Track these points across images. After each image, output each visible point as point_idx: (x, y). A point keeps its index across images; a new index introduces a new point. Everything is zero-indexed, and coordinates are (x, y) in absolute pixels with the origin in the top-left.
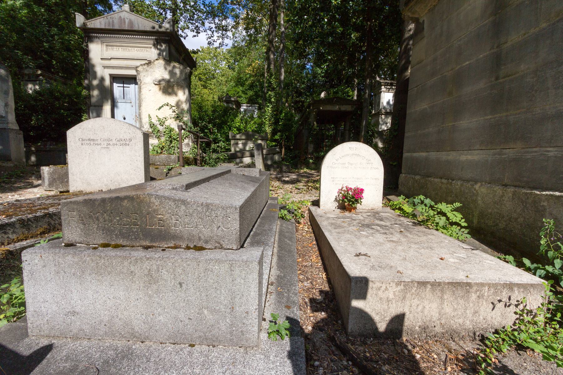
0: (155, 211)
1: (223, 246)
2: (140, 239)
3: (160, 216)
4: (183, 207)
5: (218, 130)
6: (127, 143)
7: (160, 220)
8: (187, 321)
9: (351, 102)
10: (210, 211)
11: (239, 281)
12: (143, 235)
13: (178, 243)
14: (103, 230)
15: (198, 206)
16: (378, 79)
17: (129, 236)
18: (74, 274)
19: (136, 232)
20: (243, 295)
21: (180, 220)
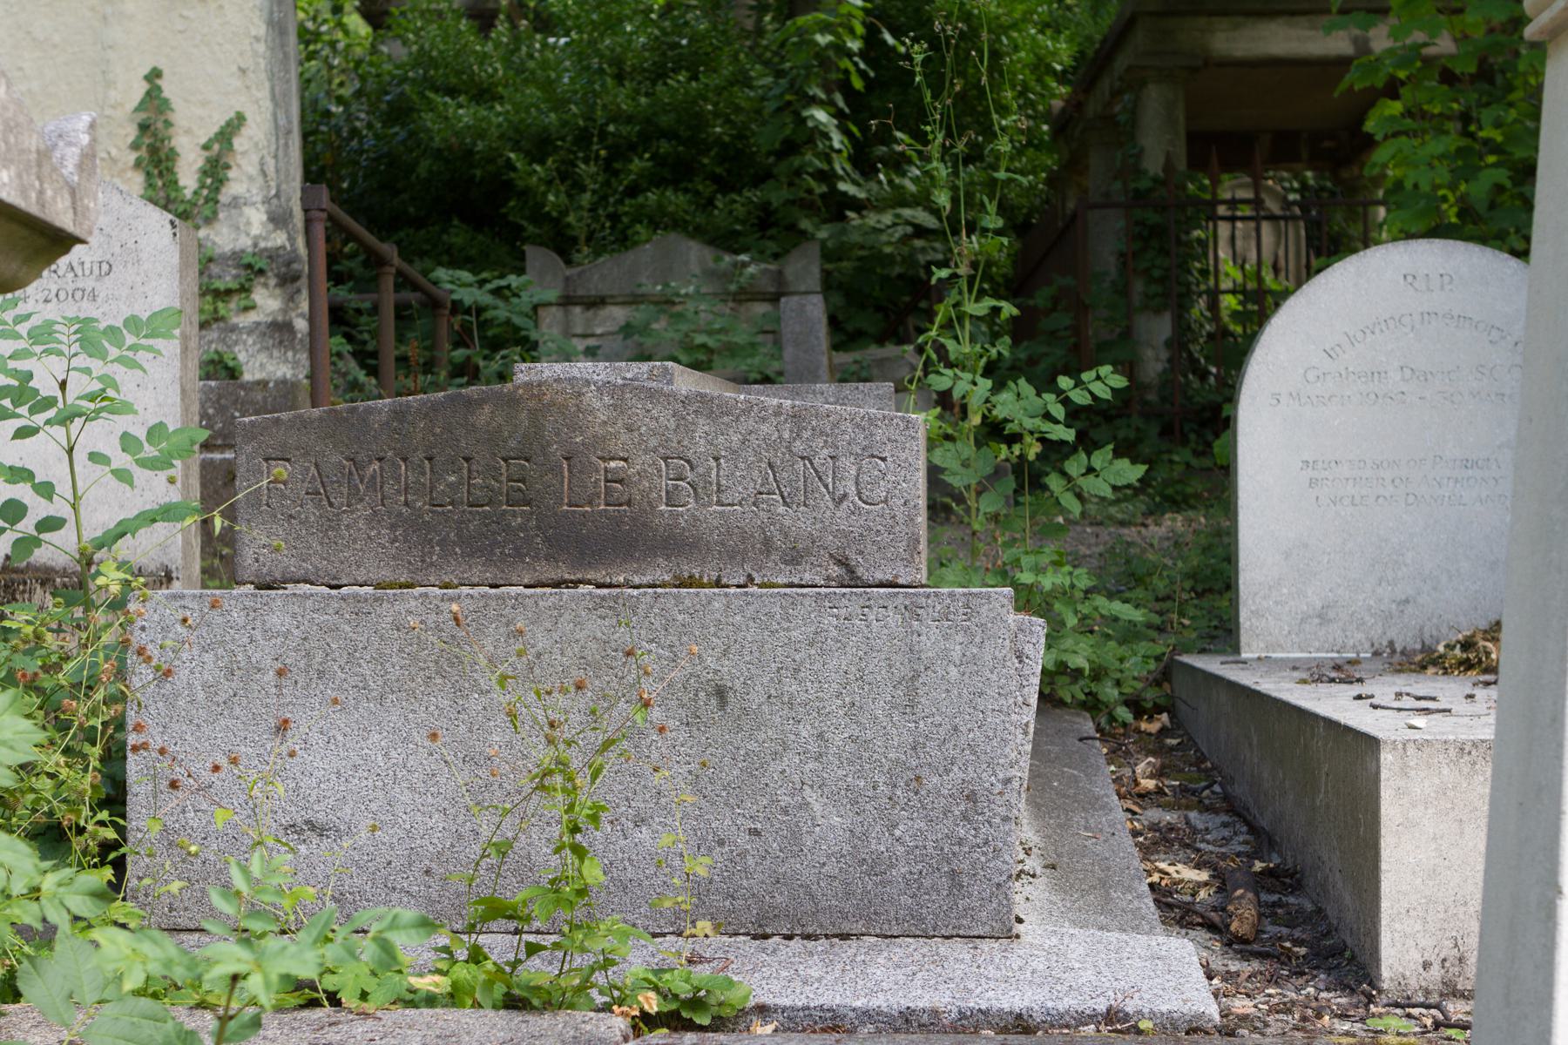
0: (599, 440)
1: (860, 571)
2: (536, 558)
3: (613, 464)
4: (703, 426)
5: (883, 144)
6: (89, 284)
7: (614, 478)
8: (743, 840)
9: (936, 212)
10: (806, 434)
11: (941, 672)
12: (547, 540)
13: (688, 569)
14: (393, 527)
15: (764, 420)
16: (501, 73)
17: (495, 544)
18: (321, 674)
19: (521, 528)
20: (956, 729)
21: (690, 475)
